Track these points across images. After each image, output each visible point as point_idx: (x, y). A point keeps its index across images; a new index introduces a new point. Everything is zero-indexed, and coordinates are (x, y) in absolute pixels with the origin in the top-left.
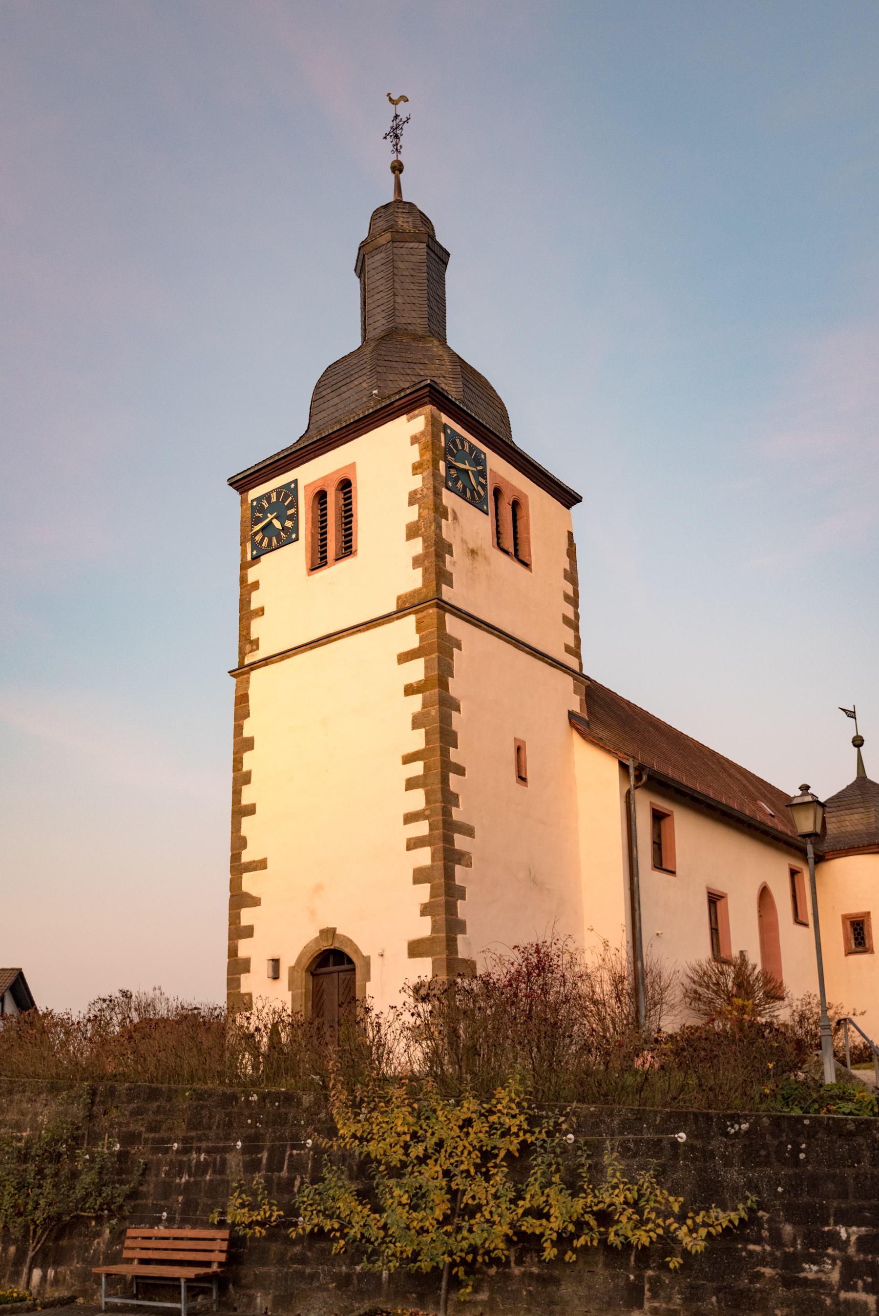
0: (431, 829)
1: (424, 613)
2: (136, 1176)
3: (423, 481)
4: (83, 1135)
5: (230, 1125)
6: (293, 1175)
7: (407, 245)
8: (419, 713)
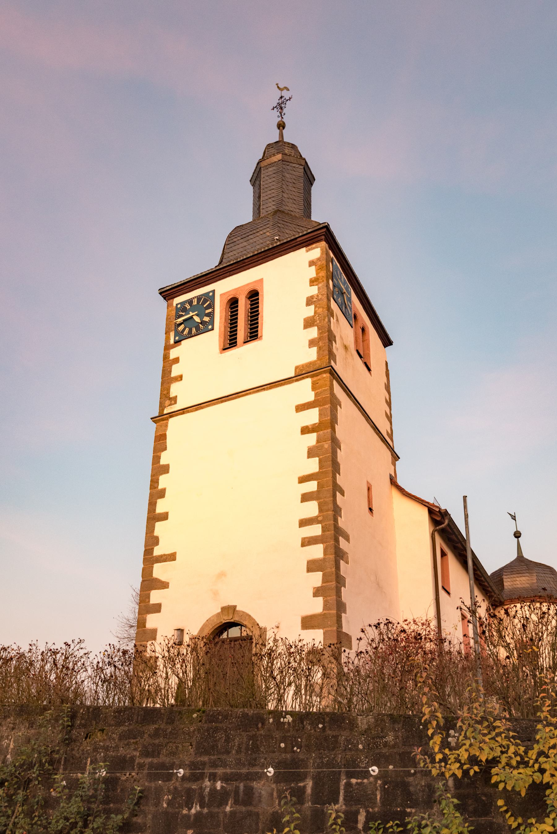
0: (323, 531)
1: (319, 377)
2: (127, 806)
3: (318, 290)
4: (60, 759)
5: (255, 749)
6: (354, 808)
7: (291, 164)
8: (314, 446)
